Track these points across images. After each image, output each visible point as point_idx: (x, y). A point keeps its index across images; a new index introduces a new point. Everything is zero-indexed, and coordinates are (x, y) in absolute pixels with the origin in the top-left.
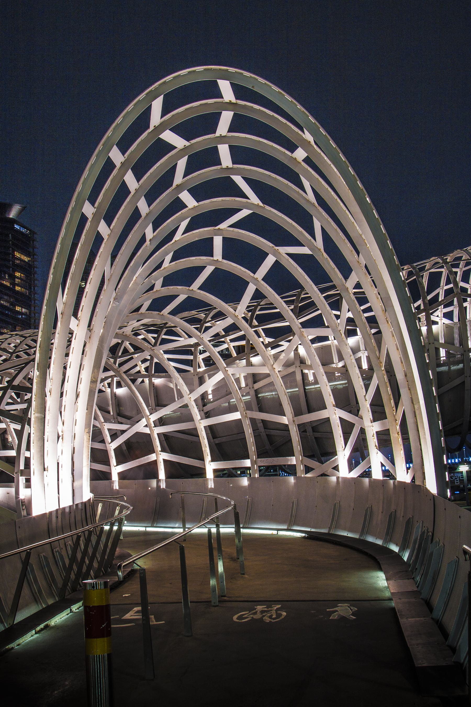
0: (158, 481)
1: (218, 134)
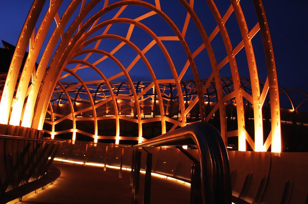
0: (72, 141)
1: (157, 37)
